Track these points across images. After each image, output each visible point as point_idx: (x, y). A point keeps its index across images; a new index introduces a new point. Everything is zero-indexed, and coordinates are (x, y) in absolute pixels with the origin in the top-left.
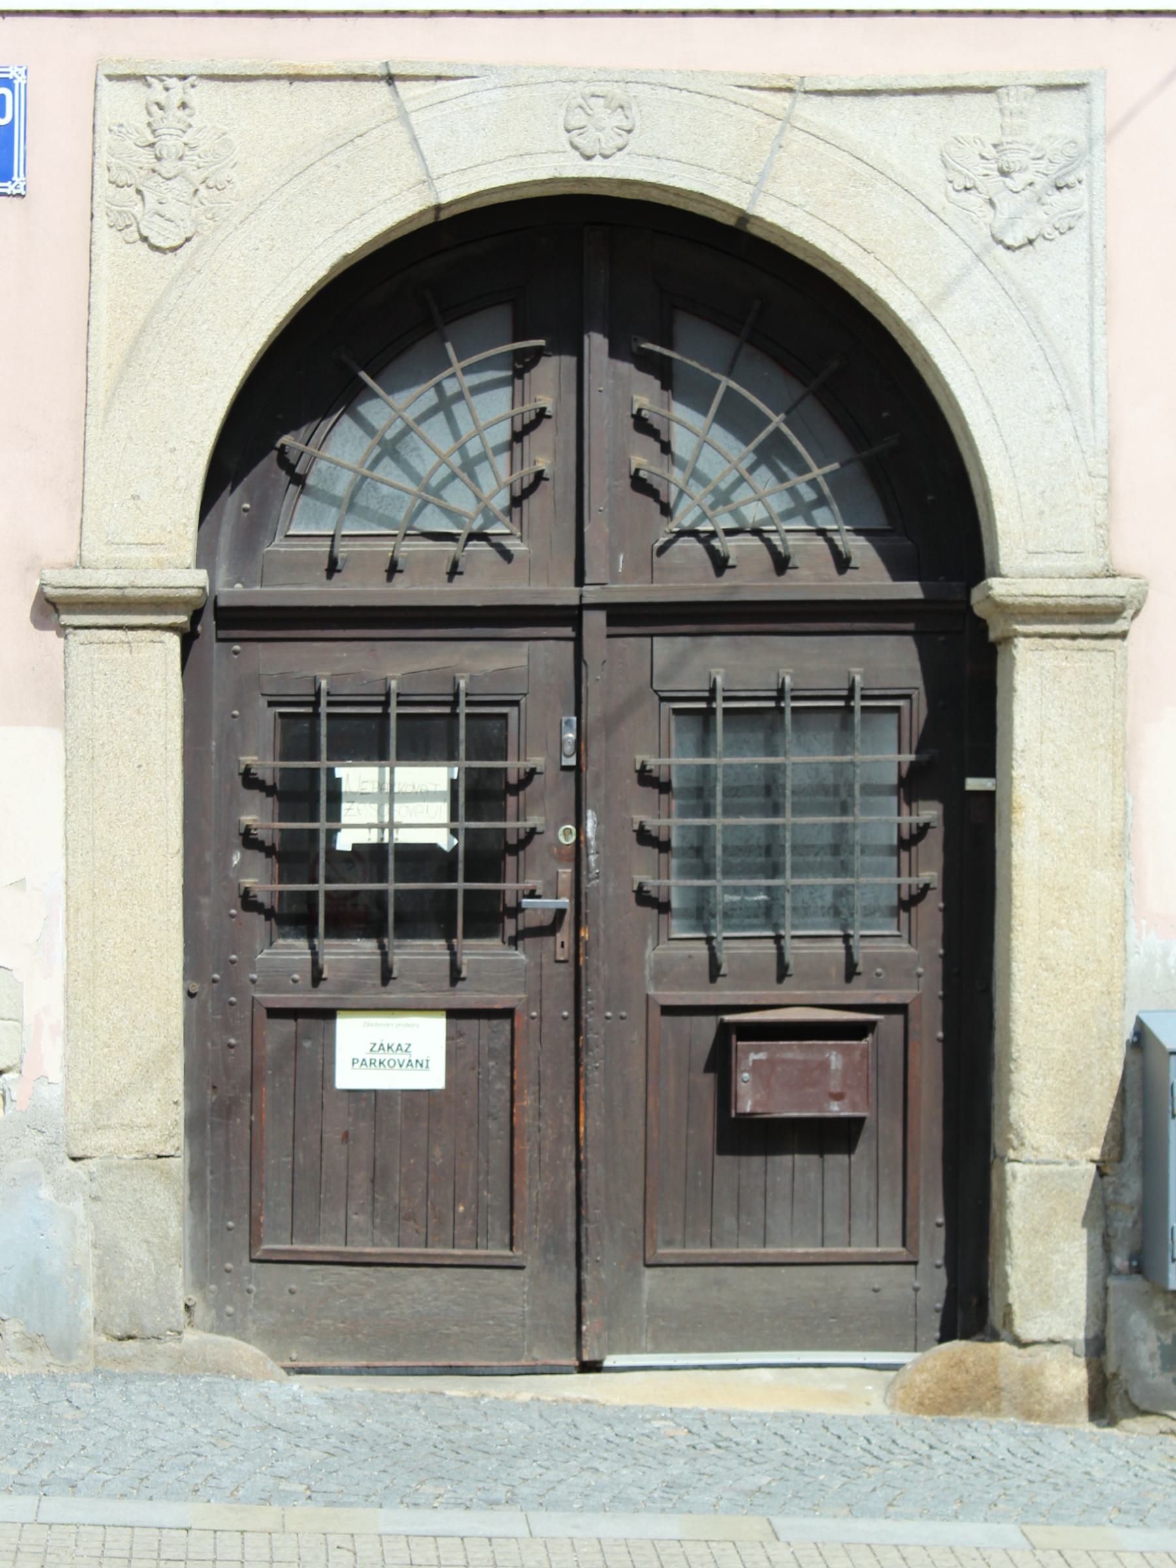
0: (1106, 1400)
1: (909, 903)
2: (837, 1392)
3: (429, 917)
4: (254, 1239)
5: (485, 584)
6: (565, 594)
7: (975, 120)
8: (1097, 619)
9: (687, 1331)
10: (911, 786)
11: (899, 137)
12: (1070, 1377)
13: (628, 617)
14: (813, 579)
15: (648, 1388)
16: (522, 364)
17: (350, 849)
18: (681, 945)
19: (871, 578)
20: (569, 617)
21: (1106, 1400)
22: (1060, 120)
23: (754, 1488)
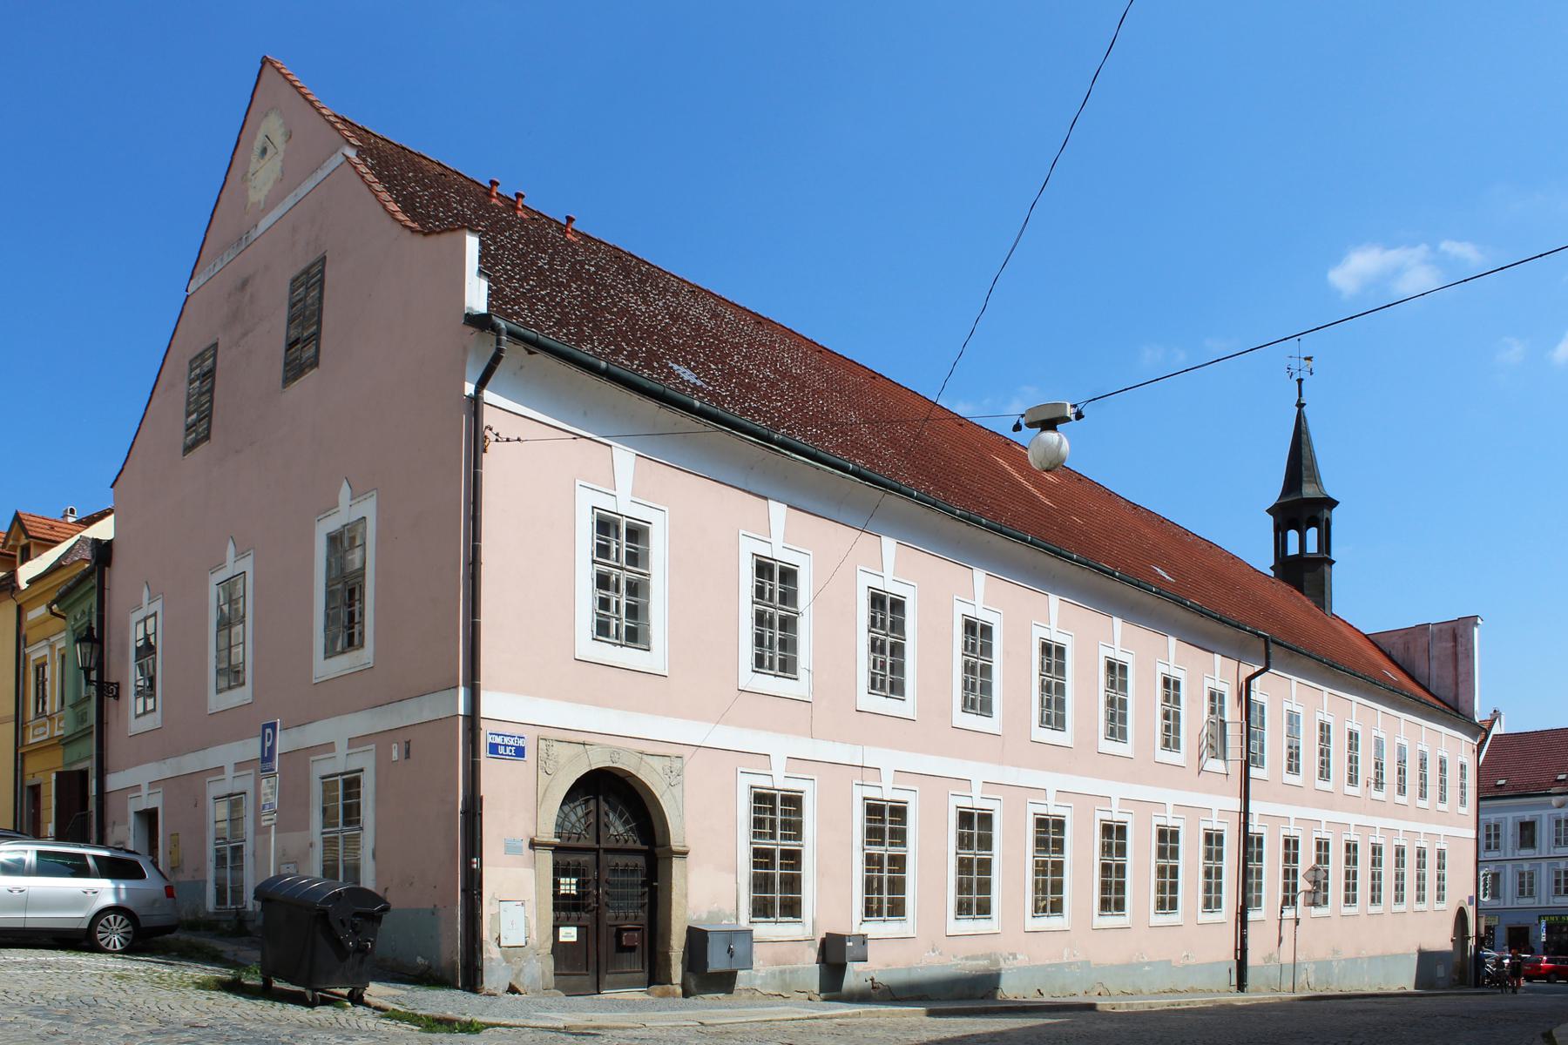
0: (686, 994)
1: (643, 906)
2: (635, 995)
3: (576, 908)
4: (54, 602)
5: (582, 843)
6: (593, 844)
7: (667, 761)
8: (684, 854)
9: (614, 986)
10: (643, 884)
11: (655, 762)
12: (679, 990)
13: (607, 851)
14: (630, 845)
15: (608, 994)
16: (587, 801)
17: (1404, 980)
18: (611, 913)
19: (638, 846)
20: (597, 851)
21: (686, 994)
22: (677, 764)
23: (112, 676)
